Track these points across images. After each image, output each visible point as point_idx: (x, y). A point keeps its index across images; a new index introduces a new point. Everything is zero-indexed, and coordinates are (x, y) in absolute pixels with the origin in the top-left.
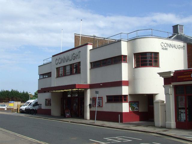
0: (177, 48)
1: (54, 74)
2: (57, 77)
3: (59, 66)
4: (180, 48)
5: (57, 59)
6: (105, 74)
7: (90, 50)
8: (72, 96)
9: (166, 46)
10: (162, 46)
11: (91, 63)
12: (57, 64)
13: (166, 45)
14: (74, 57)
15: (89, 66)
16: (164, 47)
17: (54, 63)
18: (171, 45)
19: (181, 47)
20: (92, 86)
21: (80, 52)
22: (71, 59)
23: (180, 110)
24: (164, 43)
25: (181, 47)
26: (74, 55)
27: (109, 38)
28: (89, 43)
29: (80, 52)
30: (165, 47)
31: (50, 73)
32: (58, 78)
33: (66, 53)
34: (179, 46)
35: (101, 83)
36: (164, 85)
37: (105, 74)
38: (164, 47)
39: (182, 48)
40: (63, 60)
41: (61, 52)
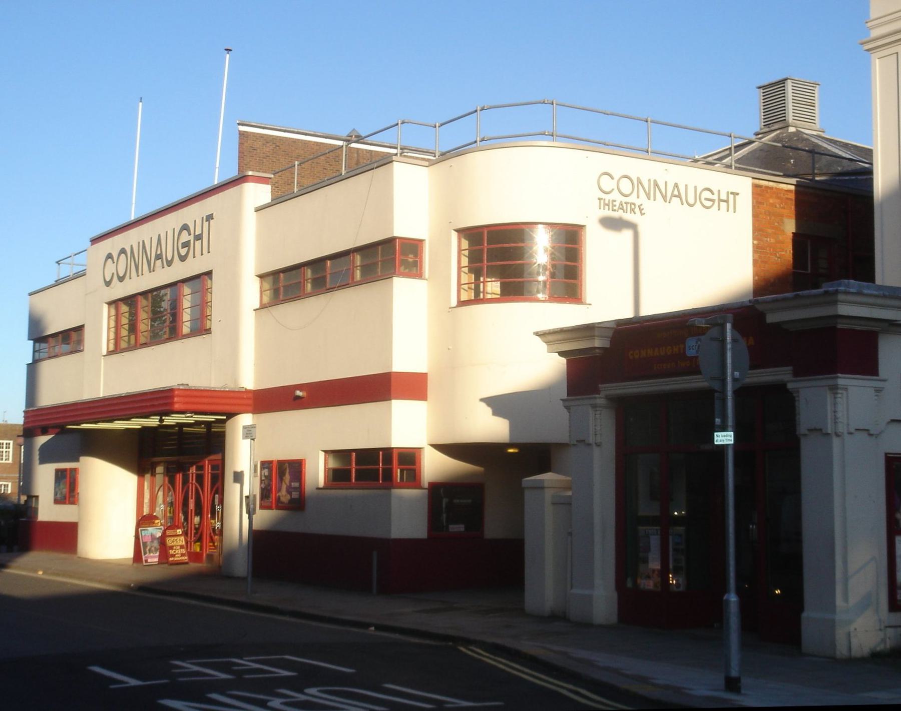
0: (691, 201)
1: (101, 331)
2: (116, 350)
3: (121, 290)
4: (708, 204)
5: (110, 256)
6: (326, 338)
7: (258, 210)
8: (161, 420)
9: (627, 191)
10: (607, 190)
11: (736, 393)
12: (108, 284)
13: (626, 186)
14: (186, 245)
15: (251, 292)
16: (615, 196)
17: (95, 278)
18: (656, 185)
19: (715, 197)
20: (271, 400)
21: (210, 217)
22: (169, 259)
23: (641, 528)
24: (616, 177)
25: (715, 197)
26: (185, 237)
27: (369, 140)
28: (250, 173)
29: (210, 217)
30: (619, 199)
31: (80, 329)
32: (115, 357)
33: (180, 211)
34: (707, 194)
35: (300, 387)
36: (568, 395)
37: (326, 338)
38: (615, 196)
39: (723, 205)
40: (136, 259)
41: (133, 218)
